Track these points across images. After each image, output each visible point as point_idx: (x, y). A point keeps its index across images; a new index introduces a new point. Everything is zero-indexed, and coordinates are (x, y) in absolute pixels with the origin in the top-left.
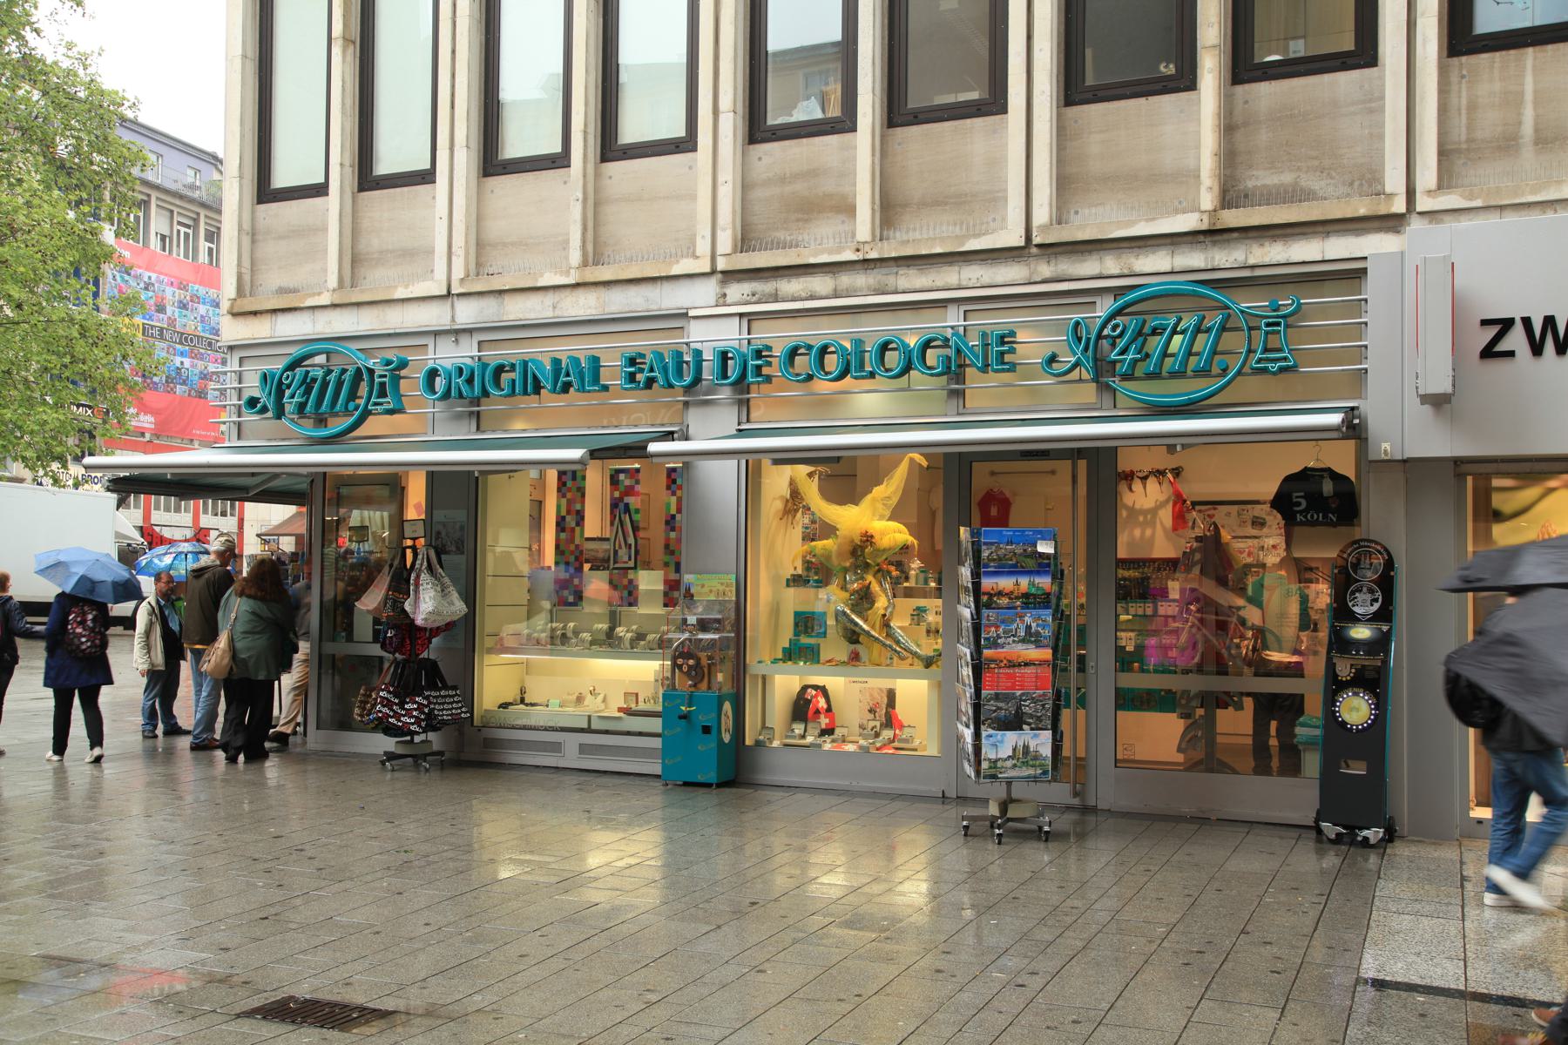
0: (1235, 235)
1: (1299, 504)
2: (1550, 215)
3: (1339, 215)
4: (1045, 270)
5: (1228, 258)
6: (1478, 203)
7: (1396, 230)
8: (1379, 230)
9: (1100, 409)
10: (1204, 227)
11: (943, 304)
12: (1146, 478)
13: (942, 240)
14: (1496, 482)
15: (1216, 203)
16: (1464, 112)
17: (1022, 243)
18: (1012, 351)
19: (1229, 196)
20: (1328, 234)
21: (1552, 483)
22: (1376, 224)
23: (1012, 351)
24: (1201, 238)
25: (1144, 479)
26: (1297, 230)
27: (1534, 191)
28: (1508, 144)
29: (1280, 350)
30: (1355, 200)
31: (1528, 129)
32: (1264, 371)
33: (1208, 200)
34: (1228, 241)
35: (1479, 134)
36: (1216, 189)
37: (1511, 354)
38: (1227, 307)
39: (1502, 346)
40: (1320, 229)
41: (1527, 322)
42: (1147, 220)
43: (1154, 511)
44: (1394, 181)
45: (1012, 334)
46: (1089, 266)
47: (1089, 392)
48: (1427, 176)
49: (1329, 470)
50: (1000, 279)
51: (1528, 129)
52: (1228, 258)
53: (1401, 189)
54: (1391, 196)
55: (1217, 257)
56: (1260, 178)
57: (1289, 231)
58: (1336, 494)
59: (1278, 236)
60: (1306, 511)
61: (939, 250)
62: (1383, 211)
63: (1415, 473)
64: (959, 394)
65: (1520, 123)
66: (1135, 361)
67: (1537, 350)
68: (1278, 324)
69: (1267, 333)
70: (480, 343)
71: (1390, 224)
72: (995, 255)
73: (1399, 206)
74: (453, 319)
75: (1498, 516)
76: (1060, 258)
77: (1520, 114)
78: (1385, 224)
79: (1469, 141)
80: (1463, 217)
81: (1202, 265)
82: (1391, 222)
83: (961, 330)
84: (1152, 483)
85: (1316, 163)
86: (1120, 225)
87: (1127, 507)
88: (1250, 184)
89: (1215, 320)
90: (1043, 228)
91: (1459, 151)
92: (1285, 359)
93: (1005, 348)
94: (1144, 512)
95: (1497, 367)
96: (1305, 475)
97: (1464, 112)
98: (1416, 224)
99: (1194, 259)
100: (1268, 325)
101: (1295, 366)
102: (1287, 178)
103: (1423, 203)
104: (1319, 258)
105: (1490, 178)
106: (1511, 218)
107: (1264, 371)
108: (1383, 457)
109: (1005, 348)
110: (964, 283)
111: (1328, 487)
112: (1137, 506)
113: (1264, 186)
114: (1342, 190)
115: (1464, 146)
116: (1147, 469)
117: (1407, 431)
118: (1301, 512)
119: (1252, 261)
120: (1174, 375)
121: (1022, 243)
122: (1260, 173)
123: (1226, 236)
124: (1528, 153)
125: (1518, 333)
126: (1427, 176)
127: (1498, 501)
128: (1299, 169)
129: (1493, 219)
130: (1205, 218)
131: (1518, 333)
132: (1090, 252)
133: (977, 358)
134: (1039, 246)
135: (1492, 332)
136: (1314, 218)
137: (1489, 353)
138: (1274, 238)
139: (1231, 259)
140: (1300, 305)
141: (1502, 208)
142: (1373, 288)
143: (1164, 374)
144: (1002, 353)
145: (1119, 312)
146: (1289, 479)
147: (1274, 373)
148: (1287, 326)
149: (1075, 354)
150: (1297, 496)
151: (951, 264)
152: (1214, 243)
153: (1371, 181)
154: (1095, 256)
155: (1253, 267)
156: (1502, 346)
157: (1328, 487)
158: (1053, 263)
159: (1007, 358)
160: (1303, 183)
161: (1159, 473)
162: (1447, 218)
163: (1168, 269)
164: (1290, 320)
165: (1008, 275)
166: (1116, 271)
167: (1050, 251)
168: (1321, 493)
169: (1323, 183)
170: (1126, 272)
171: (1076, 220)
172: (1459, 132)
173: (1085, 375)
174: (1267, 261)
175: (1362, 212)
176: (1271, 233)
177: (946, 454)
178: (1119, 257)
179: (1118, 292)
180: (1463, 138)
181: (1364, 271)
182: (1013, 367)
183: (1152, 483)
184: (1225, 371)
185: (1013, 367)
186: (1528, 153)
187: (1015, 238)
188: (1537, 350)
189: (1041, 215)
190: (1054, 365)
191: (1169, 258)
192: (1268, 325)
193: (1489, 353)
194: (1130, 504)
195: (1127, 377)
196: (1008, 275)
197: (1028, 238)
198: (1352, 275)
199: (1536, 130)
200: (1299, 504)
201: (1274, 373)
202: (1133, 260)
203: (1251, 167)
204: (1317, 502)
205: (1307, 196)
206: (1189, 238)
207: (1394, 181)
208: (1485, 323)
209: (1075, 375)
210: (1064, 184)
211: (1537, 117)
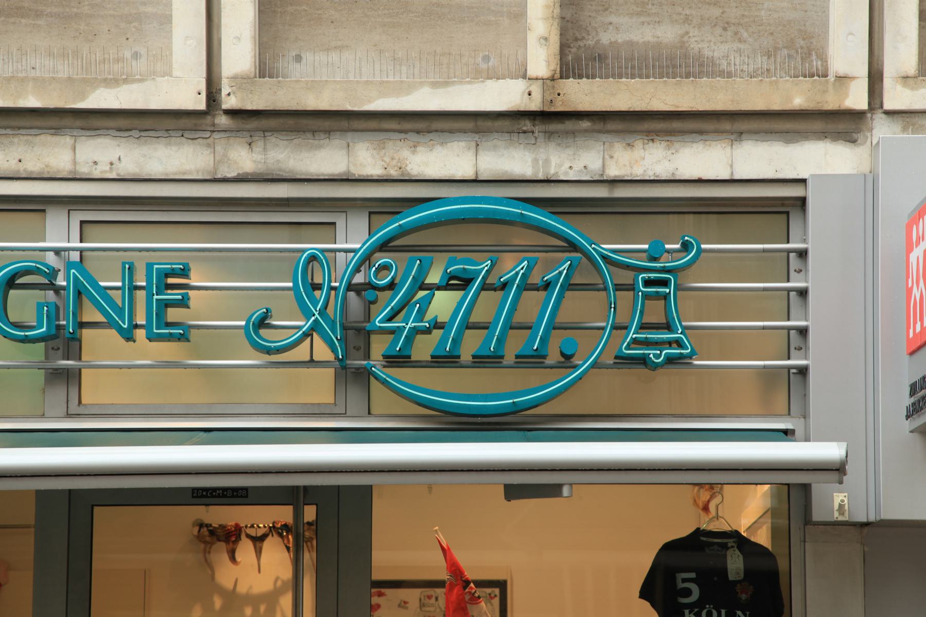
0: (585, 124)
1: (688, 593)
3: (759, 105)
4: (243, 157)
5: (575, 163)
7: (849, 138)
8: (823, 135)
9: (343, 415)
10: (535, 105)
11: (37, 206)
12: (263, 538)
13: (41, 83)
15: (555, 65)
17: (202, 106)
18: (183, 303)
19: (574, 61)
20: (739, 135)
22: (818, 125)
23: (183, 303)
24: (527, 125)
25: (258, 541)
26: (373, 124)
30: (786, 83)
32: (643, 361)
33: (541, 60)
34: (573, 133)
36: (555, 40)
40: (727, 125)
42: (435, 85)
44: (847, 54)
45: (184, 272)
46: (326, 159)
47: (320, 386)
48: (902, 50)
50: (155, 168)
52: (575, 163)
53: (862, 70)
54: (843, 79)
57: (676, 125)
61: (32, 102)
62: (831, 103)
64: (69, 379)
66: (416, 331)
68: (665, 283)
69: (646, 296)
70: (82, 222)
71: (841, 126)
72: (148, 122)
73: (857, 99)
74: (75, 162)
76: (272, 139)
78: (831, 127)
81: (529, 173)
82: (842, 124)
83: (75, 256)
86: (385, 88)
87: (223, 592)
88: (606, 38)
90: (240, 81)
93: (174, 295)
94: (254, 600)
98: (882, 130)
99: (514, 160)
100: (648, 283)
101: (690, 357)
102: (666, 34)
104: (725, 176)
108: (836, 516)
109: (174, 295)
110: (84, 170)
111: (735, 564)
112: (242, 589)
113: (631, 43)
114: (760, 61)
118: (690, 606)
119: (613, 172)
120: (482, 361)
121: (202, 106)
123: (569, 125)
128: (687, 20)
130: (536, 89)
132: (328, 132)
133: (120, 311)
134: (233, 113)
136: (719, 106)
138: (652, 135)
139: (578, 165)
140: (700, 251)
142: (819, 231)
143: (509, 359)
144: (168, 304)
145: (384, 246)
146: (669, 548)
149: (307, 314)
150: (685, 579)
151: (57, 130)
152: (550, 135)
153: (805, 51)
154: (338, 141)
155: (614, 182)
157: (735, 564)
158: (259, 145)
159: (173, 314)
160: (694, 46)
163: (469, 174)
165: (172, 160)
166: (375, 171)
167: (253, 123)
168: (724, 571)
169: (724, 48)
170: (394, 173)
171: (296, 71)
173: (322, 352)
174: (638, 172)
175: (798, 102)
177: (39, 493)
178: (381, 147)
179: (380, 209)
181: (802, 202)
182: (182, 335)
185: (182, 335)
187: (187, 94)
189: (238, 56)
190: (262, 332)
191: (470, 155)
192: (648, 283)
194: (228, 584)
195: (397, 360)
196: (172, 160)
197: (213, 96)
198: (781, 207)
200: (688, 593)
202: (405, 153)
205: (675, 64)
206: (506, 123)
207: (847, 54)
209: (301, 353)
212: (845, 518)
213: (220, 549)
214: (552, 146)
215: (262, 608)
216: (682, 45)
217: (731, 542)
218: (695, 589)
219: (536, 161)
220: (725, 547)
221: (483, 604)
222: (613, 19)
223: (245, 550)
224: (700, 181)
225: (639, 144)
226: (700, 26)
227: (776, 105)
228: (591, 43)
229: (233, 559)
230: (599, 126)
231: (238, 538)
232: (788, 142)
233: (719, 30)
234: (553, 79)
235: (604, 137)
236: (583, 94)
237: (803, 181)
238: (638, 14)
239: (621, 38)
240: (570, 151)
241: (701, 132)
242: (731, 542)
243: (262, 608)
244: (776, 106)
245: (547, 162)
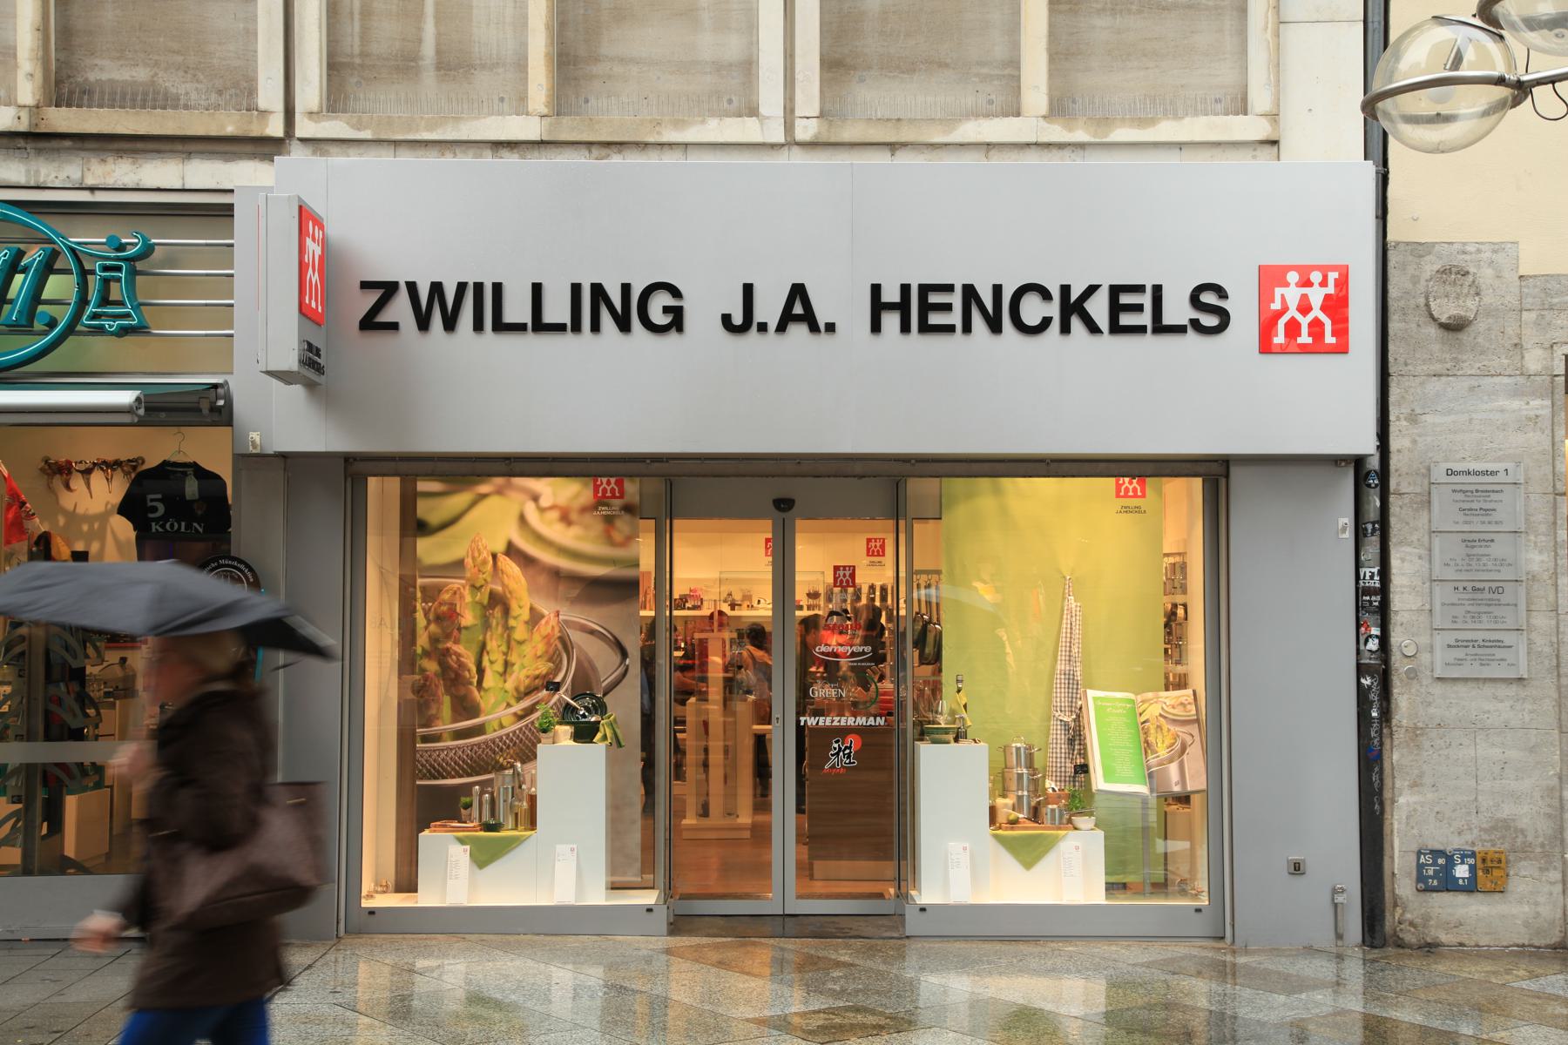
0: (68, 143)
1: (155, 509)
2: (448, 159)
3: (201, 132)
5: (60, 177)
6: (366, 134)
8: (253, 156)
14: (423, 486)
16: (357, 17)
19: (63, 87)
20: (189, 155)
21: (484, 488)
22: (249, 148)
24: (21, 143)
25: (87, 472)
26: (150, 146)
27: (430, 129)
28: (406, 65)
29: (121, 303)
31: (428, 49)
33: (27, 91)
34: (58, 150)
35: (375, 48)
36: (39, 75)
37: (394, 326)
38: (51, 241)
39: (385, 316)
40: (179, 147)
41: (412, 287)
43: (103, 518)
44: (270, 95)
48: (310, 93)
49: (195, 466)
51: (428, 49)
52: (60, 177)
53: (279, 106)
54: (264, 114)
55: (43, 171)
56: (104, 70)
57: (140, 145)
58: (203, 497)
59: (125, 151)
60: (164, 518)
63: (294, 467)
65: (420, 41)
67: (423, 323)
68: (119, 269)
73: (275, 128)
75: (423, 528)
77: (420, 29)
79: (363, 54)
80: (352, 150)
81: (23, 181)
82: (265, 148)
84: (97, 478)
85: (180, 59)
88: (92, 76)
89: (34, 255)
91: (350, 66)
92: (127, 316)
94: (87, 518)
95: (378, 342)
96: (166, 470)
97: (357, 17)
100: (106, 269)
102: (141, 74)
103: (304, 128)
105: (386, 106)
106: (406, 158)
107: (100, 330)
108: (251, 450)
111: (192, 488)
112: (80, 511)
113: (110, 80)
115: (357, 61)
116: (91, 458)
117: (282, 421)
118: (157, 520)
119: (90, 181)
122: (106, 63)
123: (54, 144)
124: (429, 78)
125: (403, 298)
126: (310, 93)
127: (425, 510)
128: (157, 64)
129: (382, 160)
130: (24, 115)
131: (403, 298)
135: (373, 297)
136: (169, 132)
137: (369, 323)
138: (120, 153)
139: (63, 175)
141: (396, 143)
147: (112, 334)
148: (133, 273)
150: (154, 499)
152: (39, 151)
153: (244, 91)
155: (92, 189)
156: (385, 316)
157: (192, 488)
161: (110, 466)
162: (333, 149)
164: (139, 266)
172: (352, 42)
174: (110, 182)
175: (230, 130)
176: (116, 145)
180: (357, 50)
181: (230, 207)
183: (97, 478)
184: (52, 324)
186: (429, 78)
188: (423, 323)
192: (106, 269)
193: (369, 323)
194: (70, 507)
198: (216, 213)
199: (438, 52)
200: (155, 509)
201: (112, 334)
203: (597, 60)
204: (178, 507)
205: (166, 101)
207: (270, 95)
208: (365, 285)
210: (835, 66)
211: (439, 35)
212: (257, 451)
213: (57, 482)
214: (41, 159)
215: (96, 526)
216: (153, 83)
217: (190, 471)
218: (161, 509)
219: (28, 171)
220: (185, 474)
221: (37, 520)
222: (98, 61)
223: (77, 482)
224: (158, 190)
225: (110, 160)
226: (166, 70)
227: (214, 131)
228: (80, 79)
229: (68, 487)
230: (79, 145)
231: (70, 473)
232: (227, 160)
233: (181, 73)
234: (37, 107)
235: (83, 154)
236: (63, 120)
237: (232, 191)
238: (119, 58)
239: (104, 77)
240: (56, 164)
241: (159, 152)
242: (190, 471)
243: (96, 526)
244: (213, 133)
245: (37, 172)
